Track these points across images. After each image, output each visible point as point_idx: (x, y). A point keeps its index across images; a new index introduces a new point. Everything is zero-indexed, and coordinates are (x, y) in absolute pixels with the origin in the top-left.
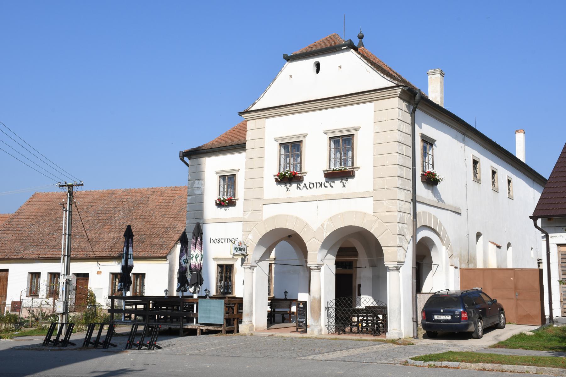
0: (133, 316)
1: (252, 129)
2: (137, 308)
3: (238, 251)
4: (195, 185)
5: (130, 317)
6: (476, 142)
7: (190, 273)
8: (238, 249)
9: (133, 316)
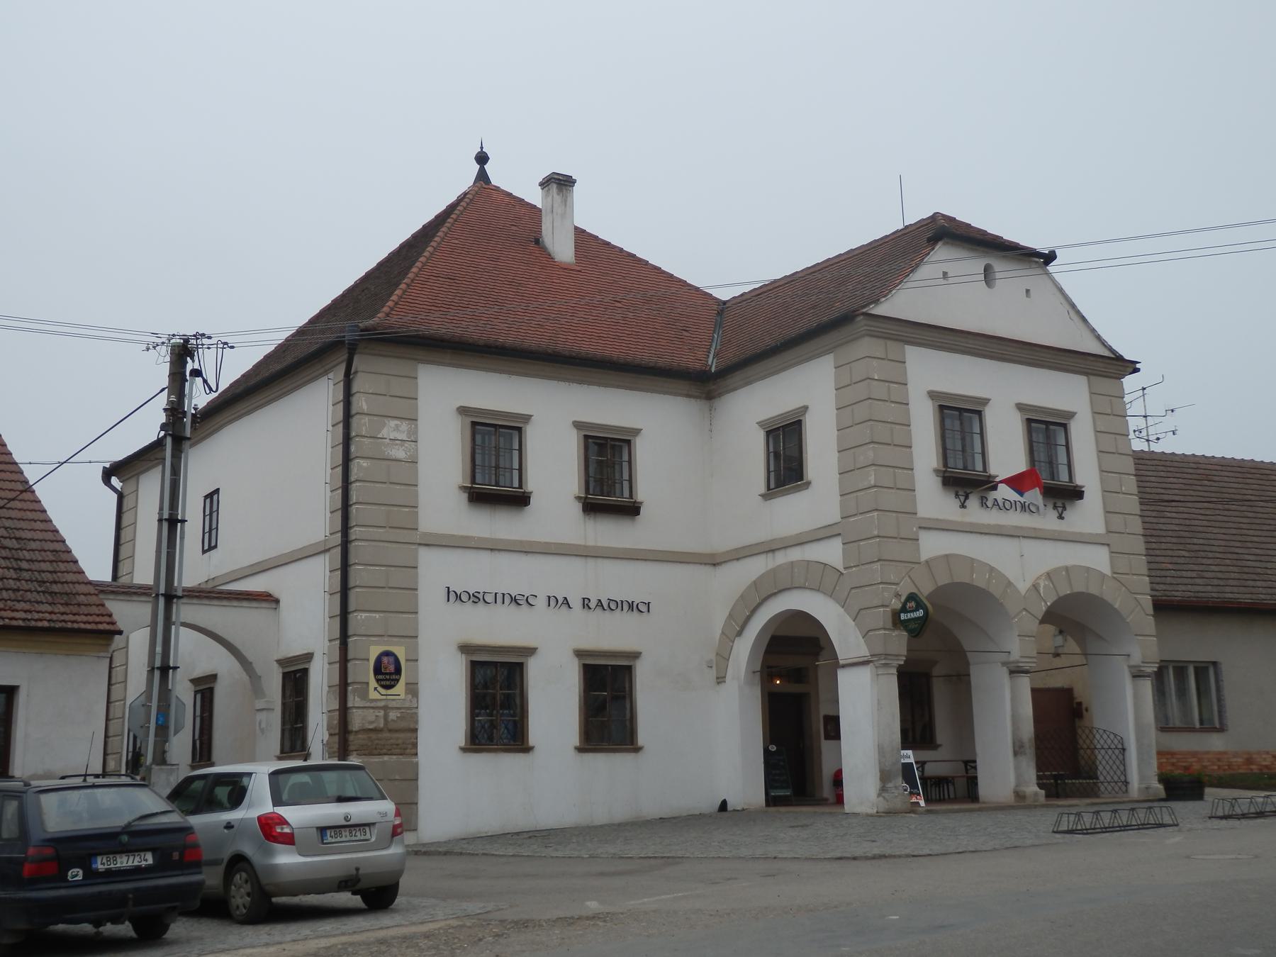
7: (376, 685)
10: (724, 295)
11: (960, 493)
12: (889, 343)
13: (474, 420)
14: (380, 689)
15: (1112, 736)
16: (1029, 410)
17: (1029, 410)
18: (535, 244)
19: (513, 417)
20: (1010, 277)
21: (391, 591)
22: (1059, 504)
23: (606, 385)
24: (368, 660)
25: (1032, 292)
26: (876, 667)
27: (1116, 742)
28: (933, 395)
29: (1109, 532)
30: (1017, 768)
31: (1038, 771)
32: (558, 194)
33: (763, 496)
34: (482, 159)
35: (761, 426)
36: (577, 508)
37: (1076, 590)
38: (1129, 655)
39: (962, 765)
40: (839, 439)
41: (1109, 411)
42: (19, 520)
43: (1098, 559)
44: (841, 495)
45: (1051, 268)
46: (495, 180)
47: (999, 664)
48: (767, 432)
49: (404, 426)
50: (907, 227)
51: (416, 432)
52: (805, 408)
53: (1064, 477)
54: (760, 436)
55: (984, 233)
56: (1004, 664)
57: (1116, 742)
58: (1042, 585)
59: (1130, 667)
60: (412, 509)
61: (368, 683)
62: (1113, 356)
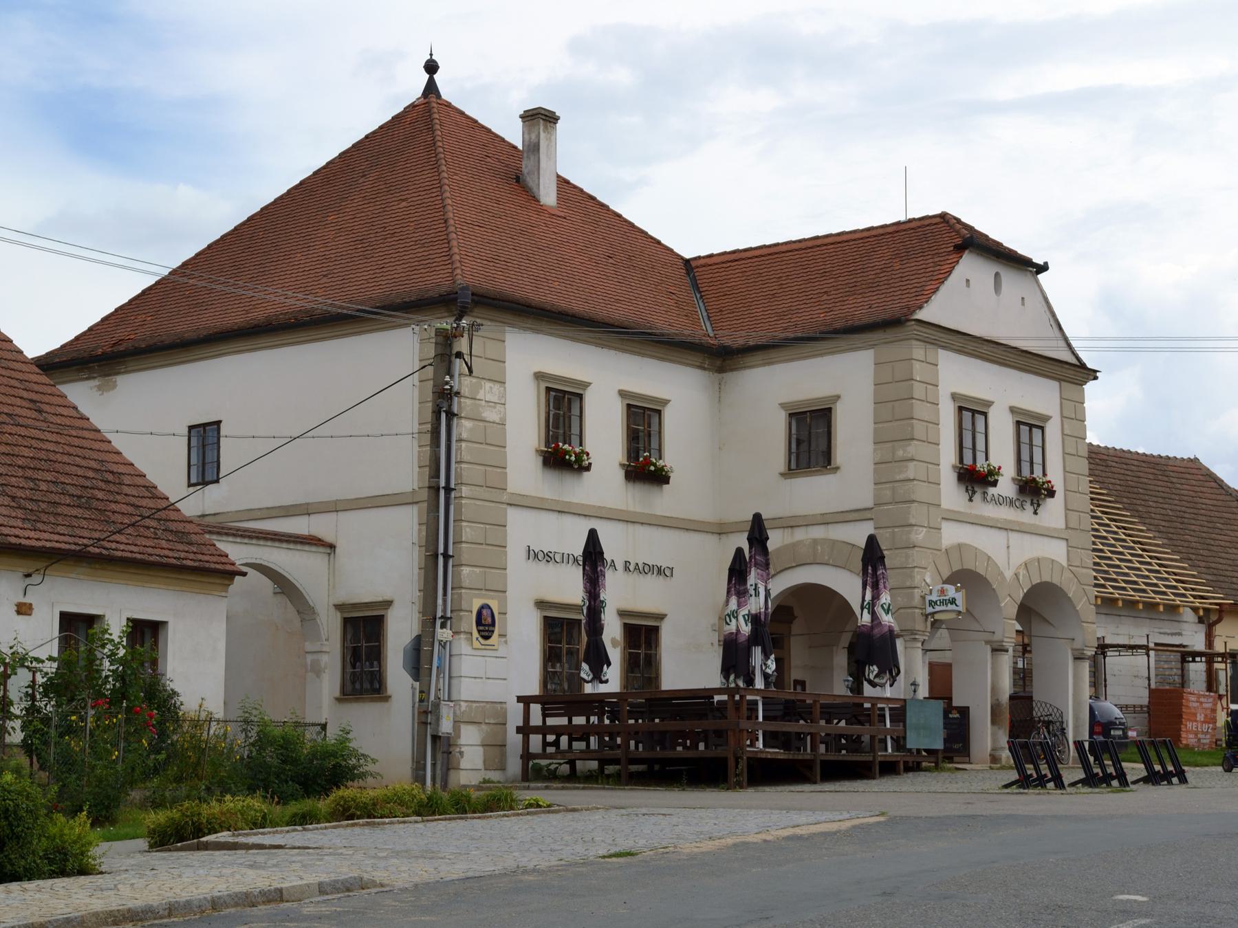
0: (564, 740)
1: (906, 397)
2: (567, 718)
3: (936, 607)
4: (482, 392)
5: (556, 743)
6: (525, 329)
7: (478, 636)
8: (936, 603)
9: (564, 740)
10: (687, 256)
11: (969, 488)
12: (928, 346)
13: (631, 403)
14: (480, 639)
15: (1055, 710)
16: (1020, 413)
17: (1020, 413)
18: (516, 182)
19: (577, 384)
20: (1013, 281)
21: (487, 547)
22: (1035, 501)
23: (603, 346)
24: (471, 612)
25: (971, 282)
26: (905, 641)
27: (1058, 715)
28: (954, 397)
29: (1067, 528)
30: (993, 734)
31: (1010, 737)
32: (544, 132)
33: (782, 475)
34: (431, 67)
35: (783, 408)
36: (621, 474)
37: (1043, 580)
38: (994, 633)
39: (323, 721)
40: (876, 431)
41: (1073, 416)
42: (106, 452)
43: (1056, 551)
44: (875, 484)
45: (1041, 277)
46: (447, 91)
47: (983, 643)
48: (790, 414)
49: (496, 387)
50: (910, 221)
51: (504, 396)
52: (838, 397)
53: (1038, 473)
54: (781, 419)
55: (999, 244)
56: (987, 642)
57: (1058, 715)
58: (1021, 574)
59: (1073, 650)
60: (499, 470)
61: (471, 634)
62: (1078, 364)
